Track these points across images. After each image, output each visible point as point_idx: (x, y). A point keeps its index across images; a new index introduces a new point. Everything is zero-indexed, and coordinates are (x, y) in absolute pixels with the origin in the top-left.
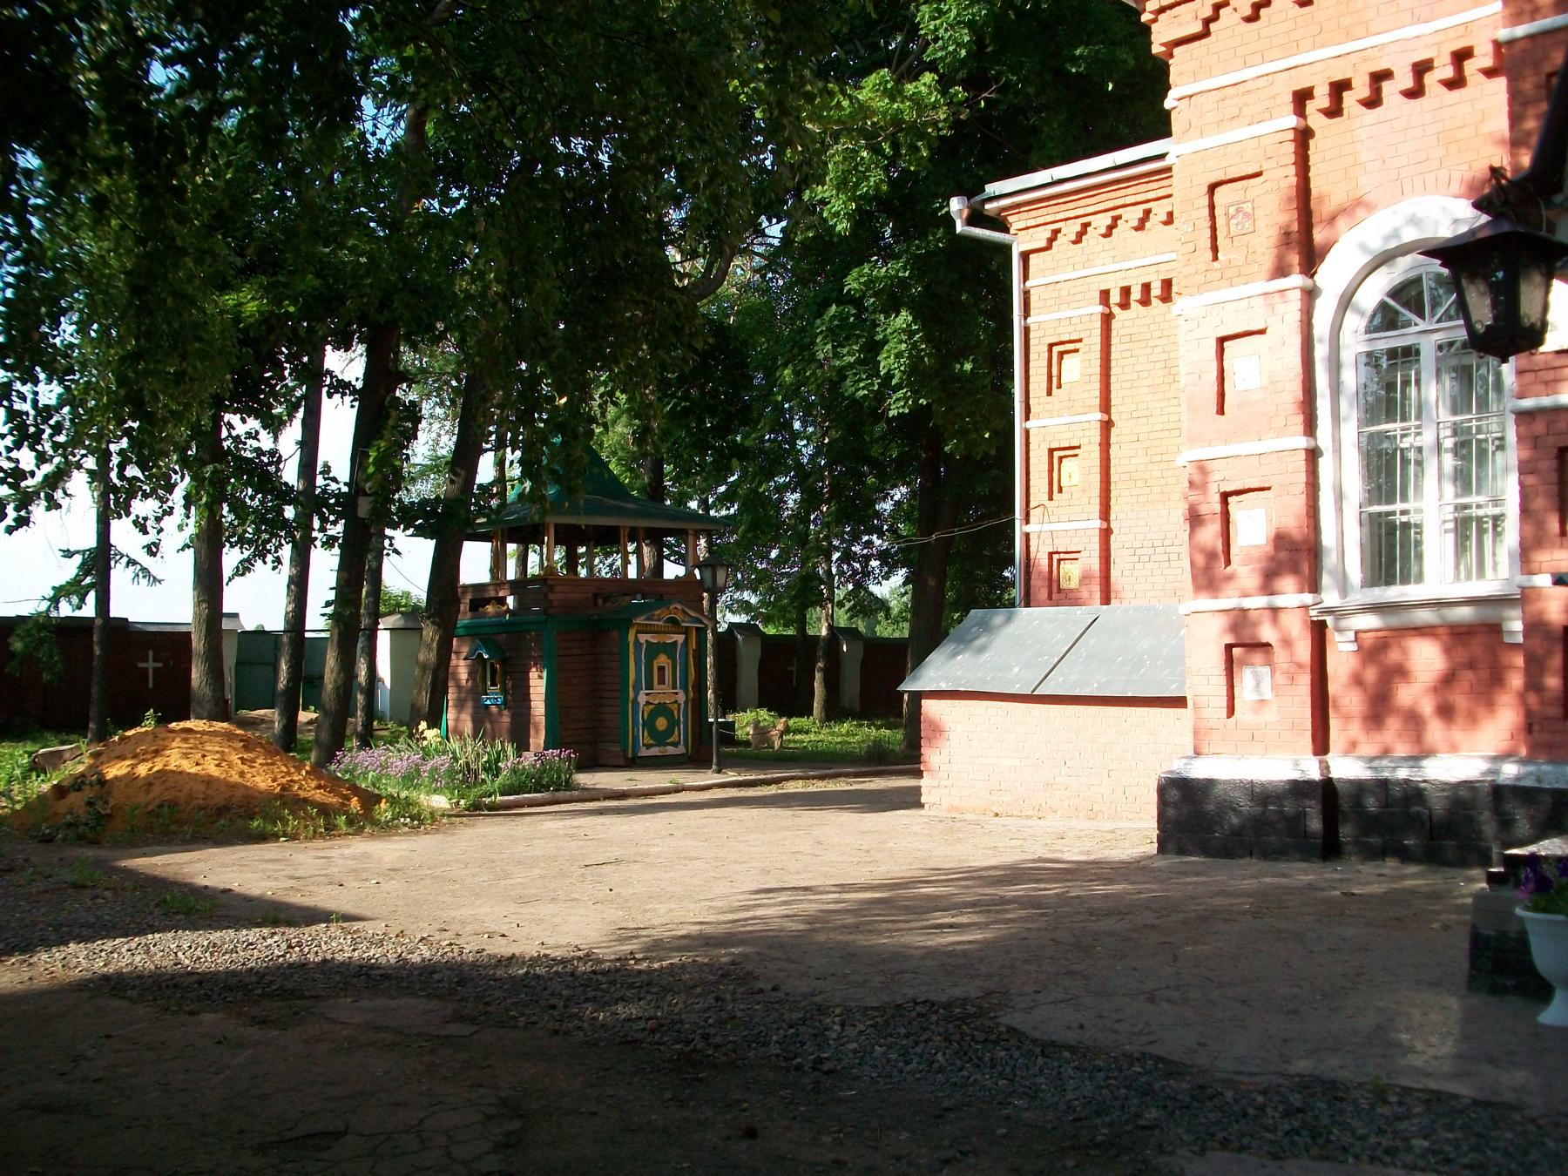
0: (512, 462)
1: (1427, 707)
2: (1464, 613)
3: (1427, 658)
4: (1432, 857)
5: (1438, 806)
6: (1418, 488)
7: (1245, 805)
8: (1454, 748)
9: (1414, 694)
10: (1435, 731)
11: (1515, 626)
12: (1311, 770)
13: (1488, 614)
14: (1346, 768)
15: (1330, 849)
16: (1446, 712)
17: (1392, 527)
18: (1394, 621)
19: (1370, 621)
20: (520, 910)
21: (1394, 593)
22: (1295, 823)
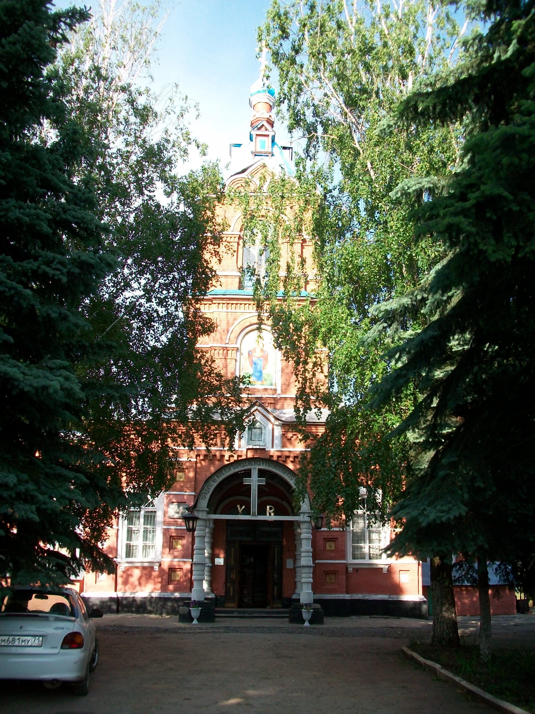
0: (67, 379)
1: (137, 583)
2: (146, 565)
3: (137, 573)
4: (138, 612)
5: (138, 602)
6: (376, 564)
7: (98, 602)
8: (142, 591)
9: (134, 579)
10: (138, 588)
11: (156, 568)
12: (114, 595)
13: (151, 565)
14: (120, 594)
15: (118, 612)
16: (140, 584)
17: (130, 546)
18: (130, 565)
19: (127, 565)
20: (21, 216)
21: (130, 559)
22: (109, 607)
